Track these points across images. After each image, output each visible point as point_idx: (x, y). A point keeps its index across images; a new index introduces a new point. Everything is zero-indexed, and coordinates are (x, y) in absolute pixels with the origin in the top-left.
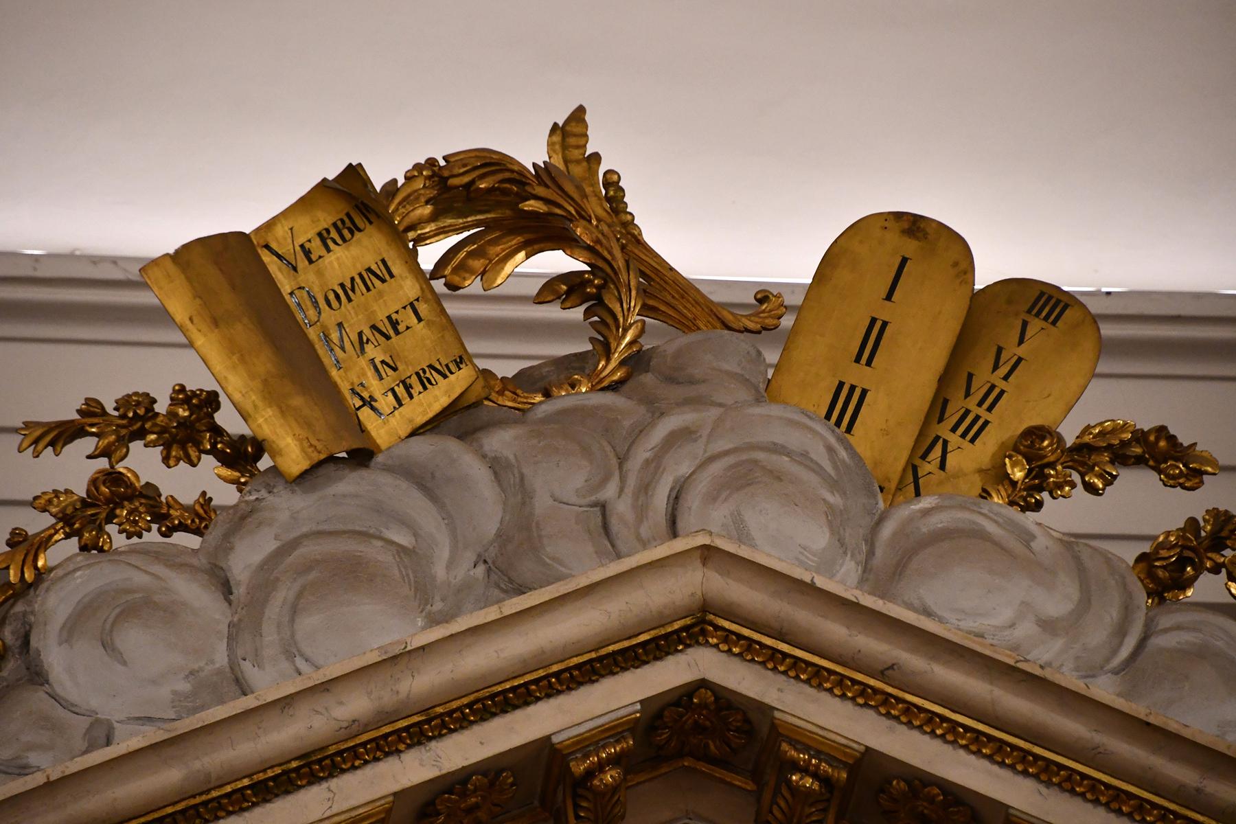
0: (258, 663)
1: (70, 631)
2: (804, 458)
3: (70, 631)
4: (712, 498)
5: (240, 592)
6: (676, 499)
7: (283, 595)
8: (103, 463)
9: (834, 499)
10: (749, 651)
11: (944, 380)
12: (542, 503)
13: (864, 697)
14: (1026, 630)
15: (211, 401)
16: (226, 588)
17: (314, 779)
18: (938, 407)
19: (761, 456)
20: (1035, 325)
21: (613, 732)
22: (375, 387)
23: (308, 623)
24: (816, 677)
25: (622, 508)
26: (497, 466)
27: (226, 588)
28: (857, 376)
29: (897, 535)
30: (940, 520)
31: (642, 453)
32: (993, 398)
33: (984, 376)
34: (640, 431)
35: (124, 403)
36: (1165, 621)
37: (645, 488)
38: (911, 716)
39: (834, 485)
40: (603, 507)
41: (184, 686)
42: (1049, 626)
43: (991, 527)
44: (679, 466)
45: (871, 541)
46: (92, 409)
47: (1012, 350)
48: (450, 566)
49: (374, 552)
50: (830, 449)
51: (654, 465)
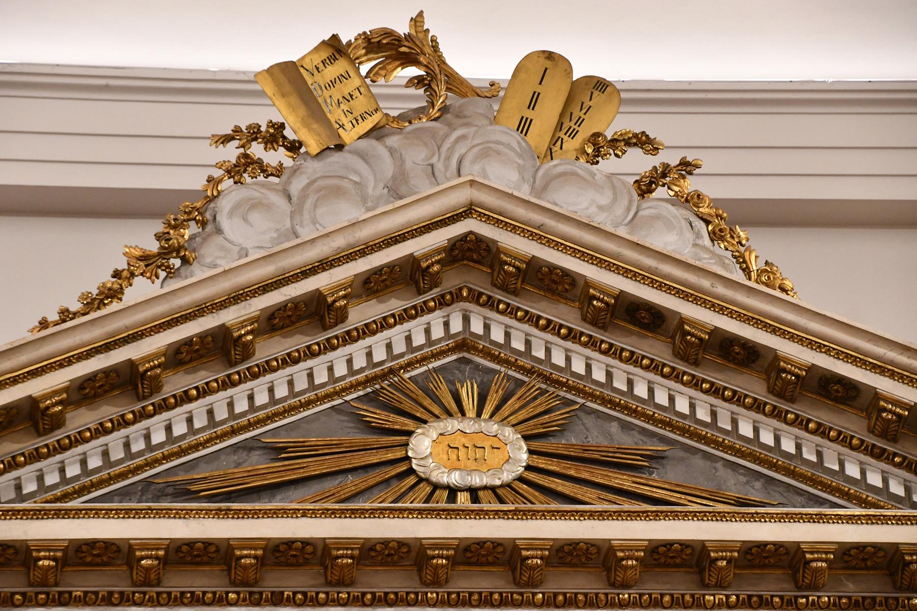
0: (302, 226)
1: (232, 213)
2: (509, 146)
3: (232, 213)
4: (474, 162)
5: (294, 199)
6: (460, 162)
7: (308, 205)
8: (242, 150)
9: (520, 162)
10: (488, 219)
11: (562, 115)
12: (409, 164)
13: (532, 236)
14: (593, 209)
15: (282, 126)
16: (289, 198)
17: (324, 270)
18: (560, 126)
19: (492, 145)
20: (596, 93)
21: (437, 251)
22: (344, 120)
23: (321, 211)
24: (514, 229)
25: (439, 166)
26: (391, 151)
27: (289, 198)
28: (529, 114)
29: (544, 175)
30: (560, 169)
31: (447, 145)
32: (580, 122)
33: (577, 113)
34: (446, 136)
35: (249, 127)
36: (645, 205)
37: (448, 158)
38: (550, 243)
39: (520, 156)
40: (432, 166)
41: (275, 235)
42: (601, 208)
43: (579, 171)
44: (461, 149)
45: (534, 178)
46: (237, 130)
47: (587, 104)
48: (374, 188)
49: (345, 184)
50: (519, 143)
51: (452, 149)
